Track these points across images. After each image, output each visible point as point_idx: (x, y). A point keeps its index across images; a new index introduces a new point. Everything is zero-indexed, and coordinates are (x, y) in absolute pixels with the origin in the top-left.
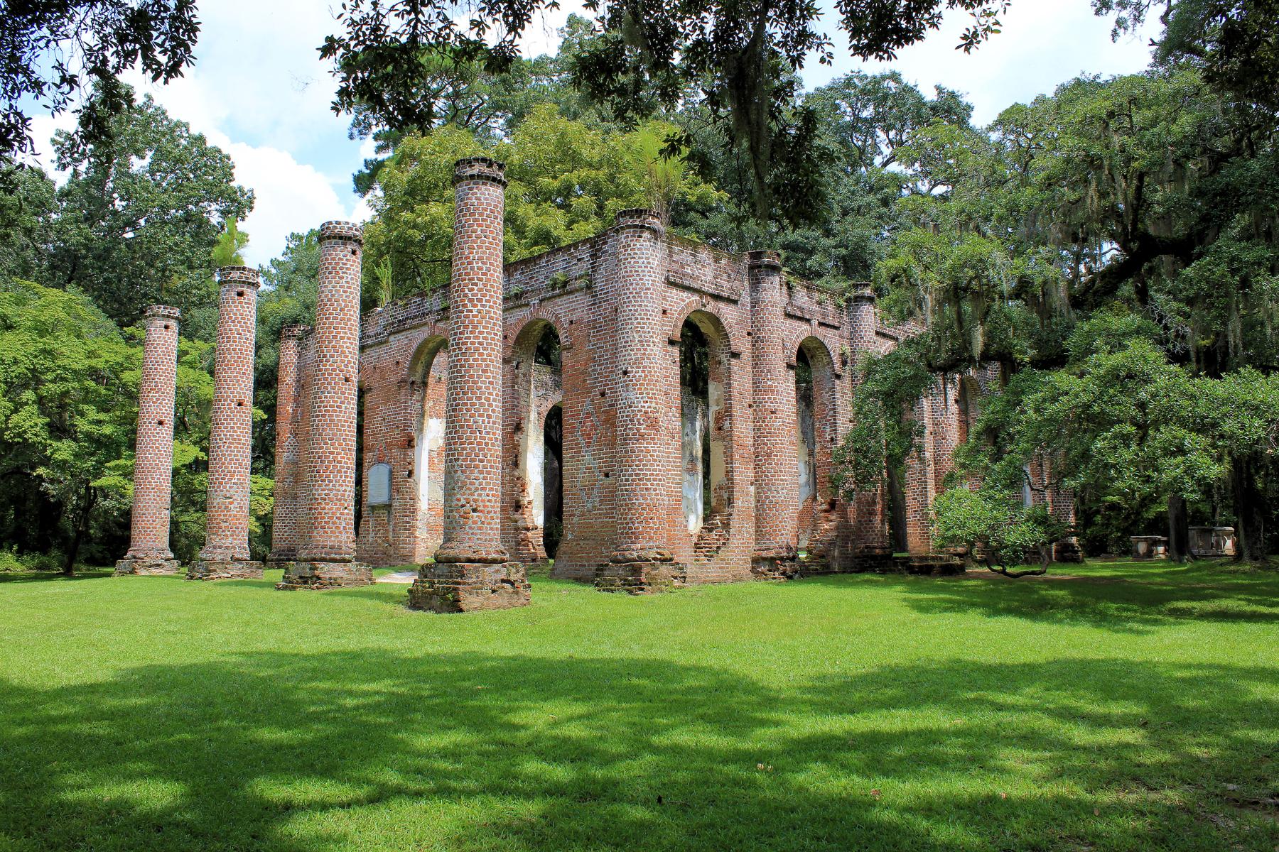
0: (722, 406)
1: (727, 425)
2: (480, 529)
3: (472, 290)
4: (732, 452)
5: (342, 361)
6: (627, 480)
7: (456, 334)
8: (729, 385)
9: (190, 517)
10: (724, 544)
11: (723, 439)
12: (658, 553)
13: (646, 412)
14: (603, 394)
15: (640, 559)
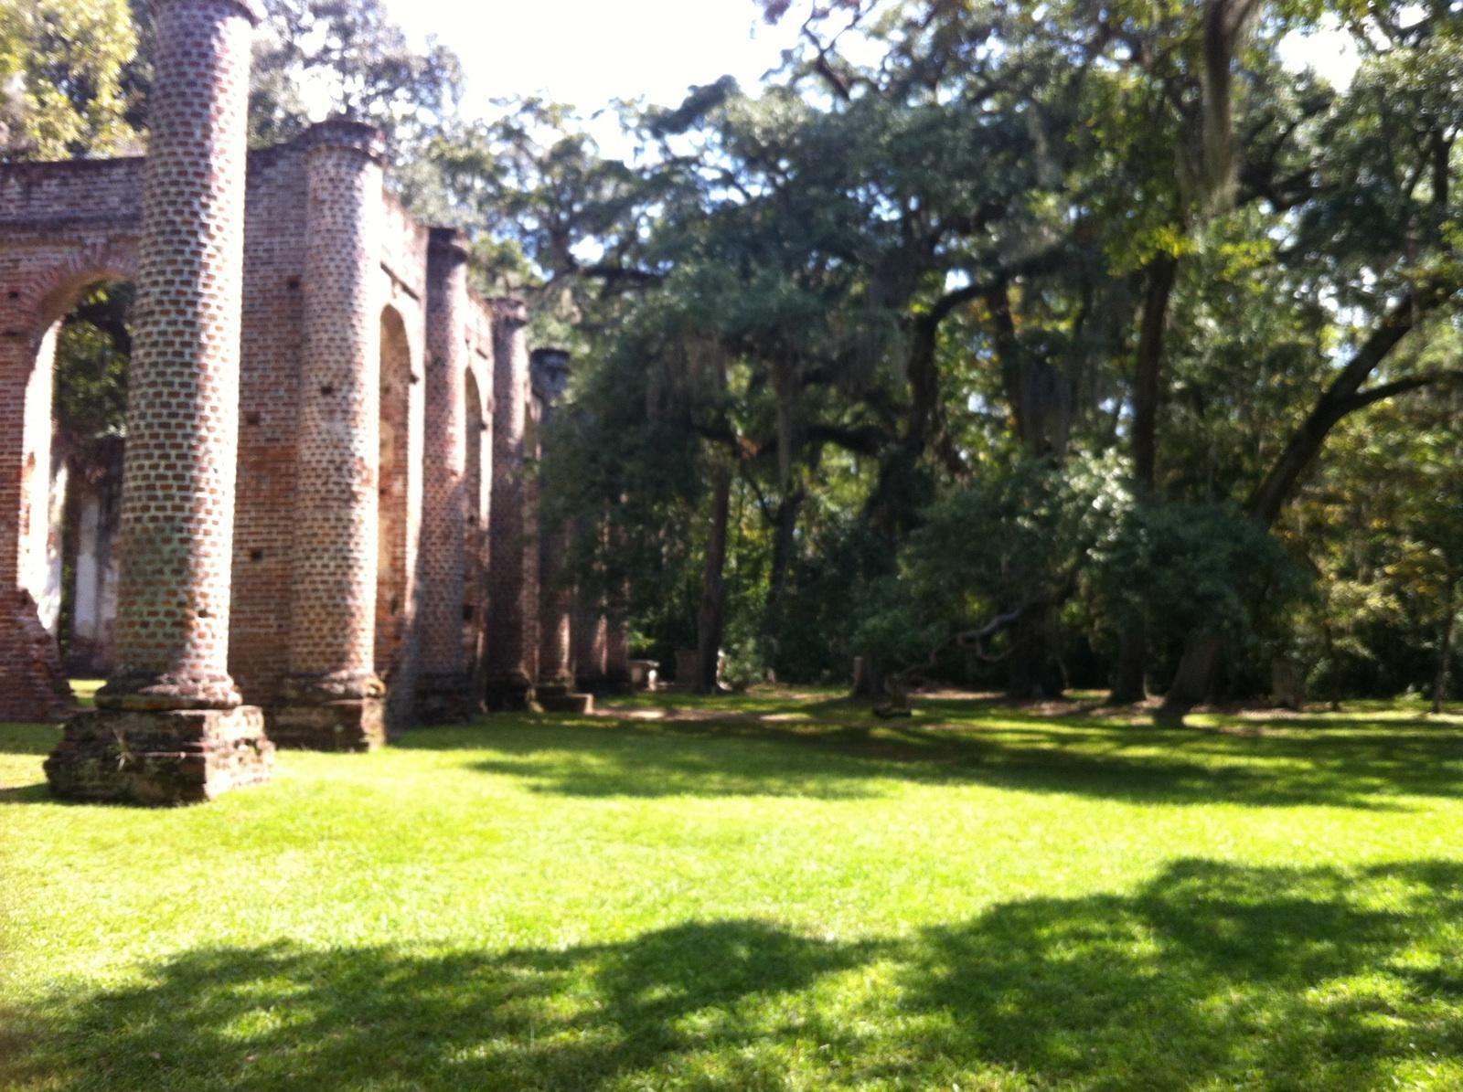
6: (326, 566)
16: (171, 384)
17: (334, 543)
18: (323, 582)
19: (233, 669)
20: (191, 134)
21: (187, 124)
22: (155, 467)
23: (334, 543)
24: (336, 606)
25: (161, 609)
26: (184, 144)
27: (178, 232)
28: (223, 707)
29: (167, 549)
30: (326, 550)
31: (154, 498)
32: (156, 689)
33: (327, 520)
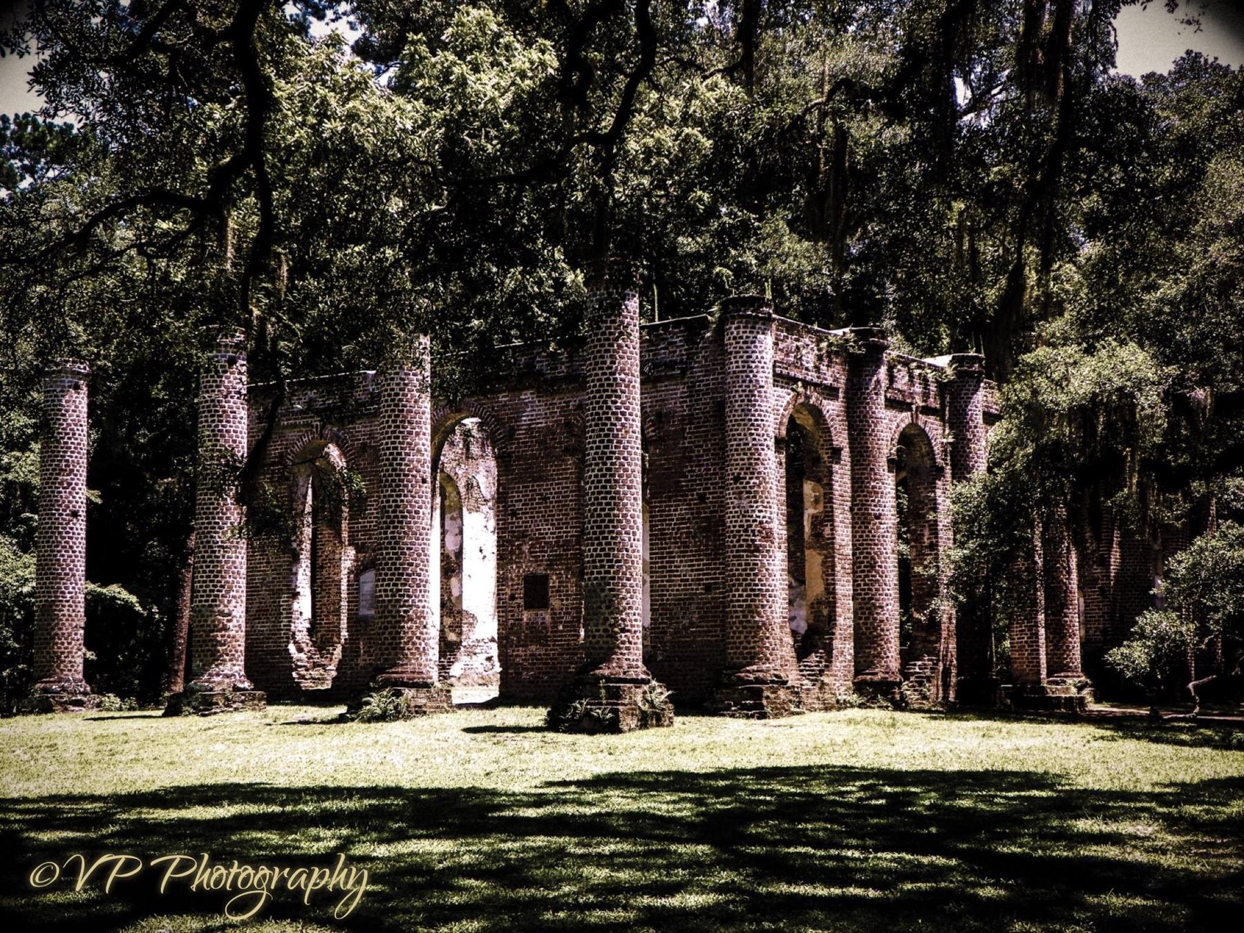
0: (820, 508)
1: (827, 531)
2: (627, 648)
3: (615, 402)
4: (833, 562)
5: (419, 461)
6: (741, 596)
7: (598, 447)
8: (830, 486)
9: (263, 627)
10: (827, 666)
11: (822, 548)
12: (776, 676)
13: (761, 523)
14: (702, 498)
15: (758, 680)
16: (601, 504)
17: (745, 580)
18: (740, 606)
19: (646, 661)
20: (605, 363)
21: (602, 357)
22: (595, 550)
23: (745, 580)
24: (749, 622)
25: (601, 628)
26: (601, 369)
27: (600, 419)
28: (638, 682)
29: (603, 595)
30: (741, 585)
31: (595, 567)
32: (597, 672)
33: (740, 565)
